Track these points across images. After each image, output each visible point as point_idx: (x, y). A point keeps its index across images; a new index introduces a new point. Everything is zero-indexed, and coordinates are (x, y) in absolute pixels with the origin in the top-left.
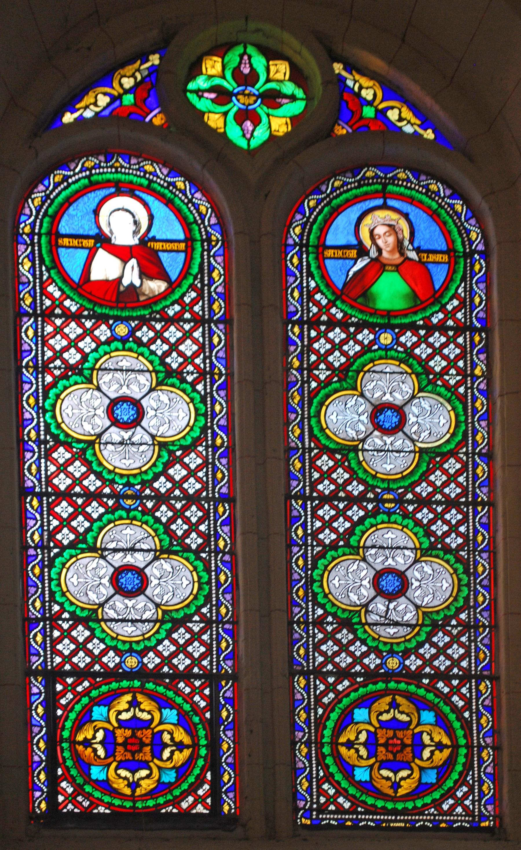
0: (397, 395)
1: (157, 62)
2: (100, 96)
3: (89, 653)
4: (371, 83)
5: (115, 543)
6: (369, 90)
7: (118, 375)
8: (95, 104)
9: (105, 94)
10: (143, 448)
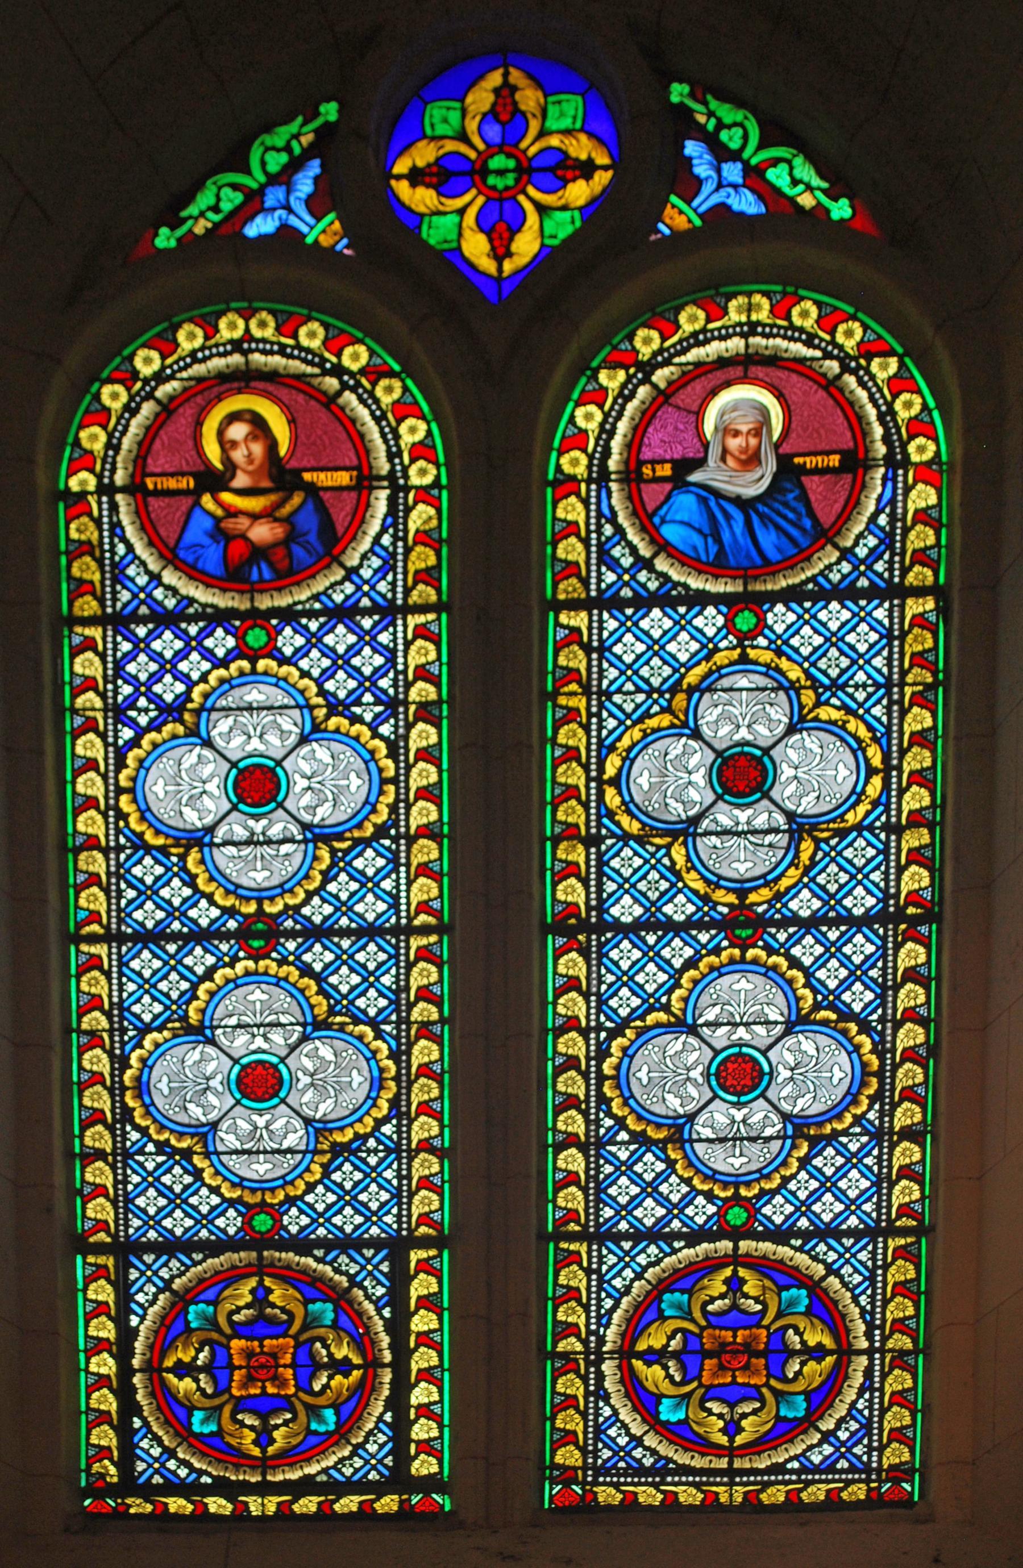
0: (761, 729)
1: (333, 117)
2: (226, 192)
3: (662, 1200)
4: (739, 116)
5: (717, 1009)
6: (734, 130)
7: (245, 718)
9: (235, 187)
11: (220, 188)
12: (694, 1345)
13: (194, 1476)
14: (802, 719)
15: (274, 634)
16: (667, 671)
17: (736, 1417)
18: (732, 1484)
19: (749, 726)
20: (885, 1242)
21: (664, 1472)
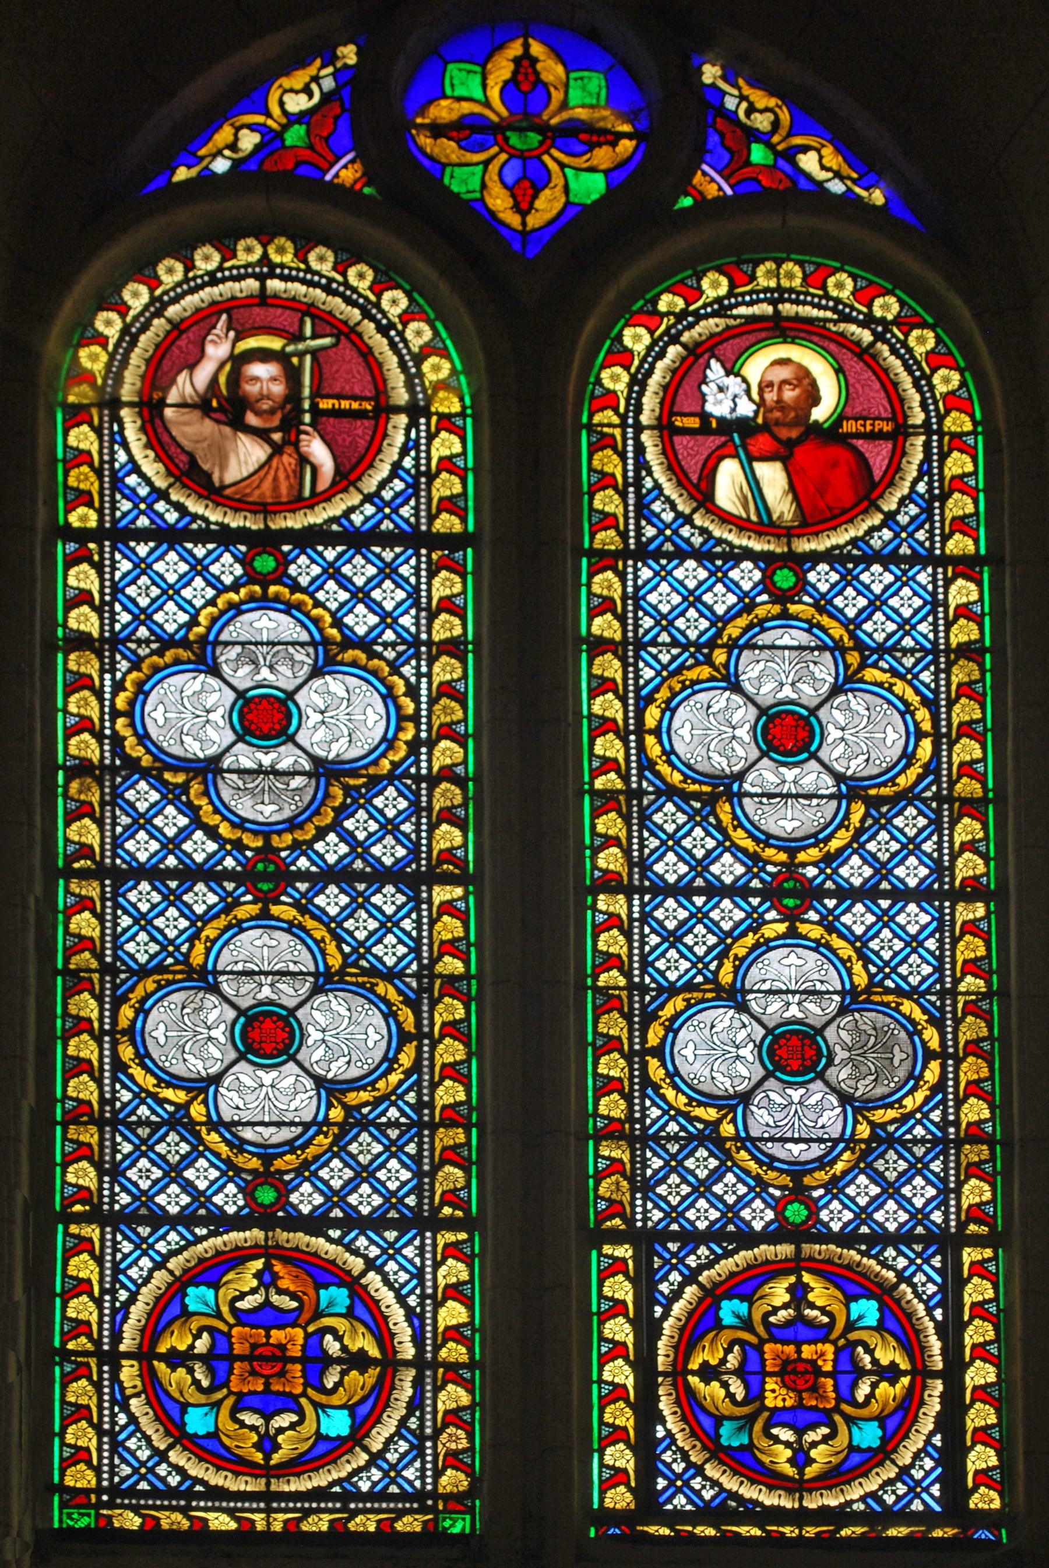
0: (807, 689)
1: (352, 60)
4: (772, 102)
8: (233, 147)
9: (253, 128)
10: (297, 782)
11: (238, 129)
12: (222, 1347)
13: (188, 1483)
14: (848, 679)
15: (284, 561)
16: (704, 624)
17: (272, 1432)
18: (269, 1511)
19: (793, 684)
20: (434, 1239)
21: (190, 1495)
